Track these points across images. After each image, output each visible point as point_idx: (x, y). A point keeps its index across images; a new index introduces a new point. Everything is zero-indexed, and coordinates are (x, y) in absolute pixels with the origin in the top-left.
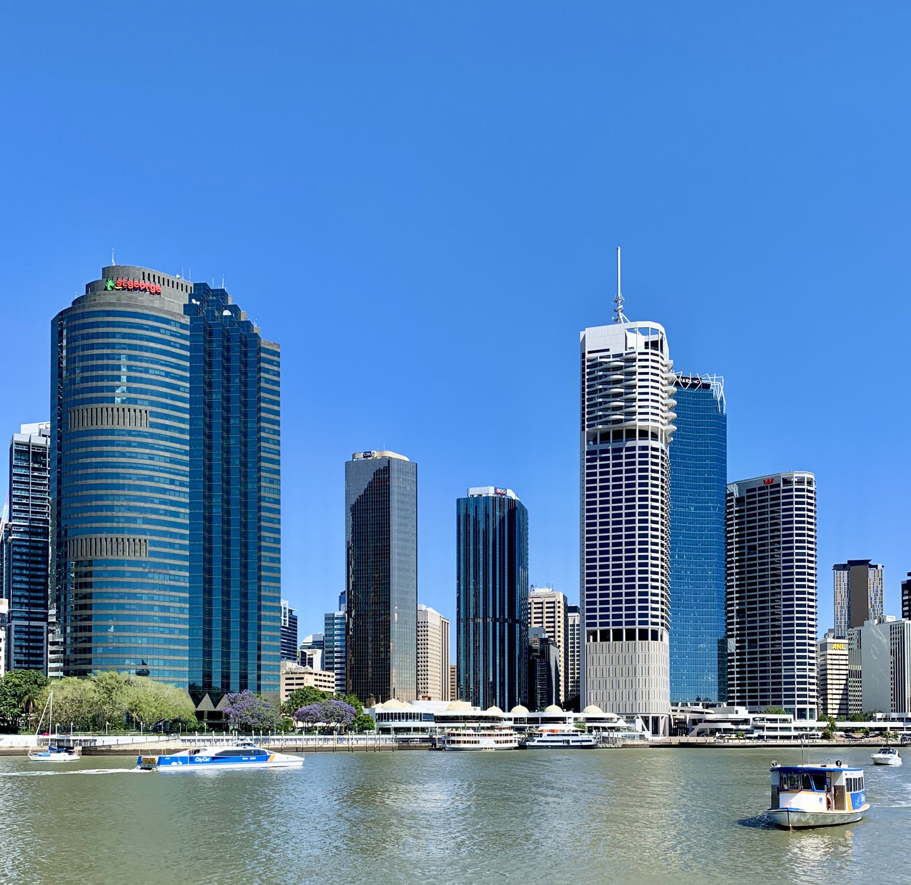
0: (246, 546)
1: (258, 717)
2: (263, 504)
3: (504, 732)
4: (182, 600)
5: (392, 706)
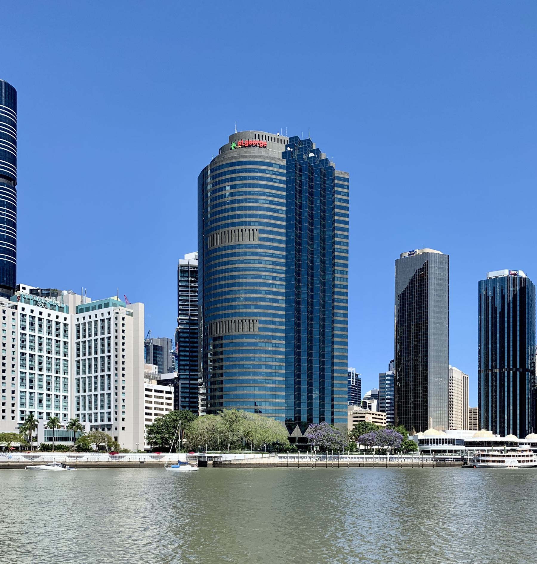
0: (324, 320)
1: (332, 441)
2: (336, 289)
3: (525, 453)
4: (281, 360)
5: (431, 433)
